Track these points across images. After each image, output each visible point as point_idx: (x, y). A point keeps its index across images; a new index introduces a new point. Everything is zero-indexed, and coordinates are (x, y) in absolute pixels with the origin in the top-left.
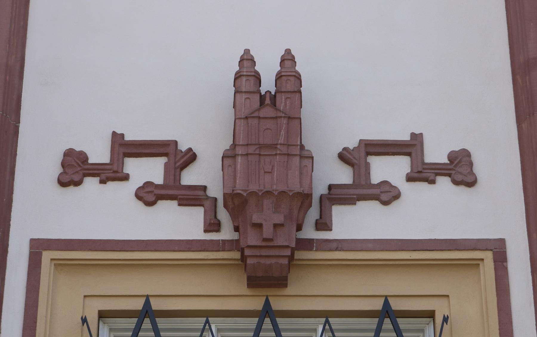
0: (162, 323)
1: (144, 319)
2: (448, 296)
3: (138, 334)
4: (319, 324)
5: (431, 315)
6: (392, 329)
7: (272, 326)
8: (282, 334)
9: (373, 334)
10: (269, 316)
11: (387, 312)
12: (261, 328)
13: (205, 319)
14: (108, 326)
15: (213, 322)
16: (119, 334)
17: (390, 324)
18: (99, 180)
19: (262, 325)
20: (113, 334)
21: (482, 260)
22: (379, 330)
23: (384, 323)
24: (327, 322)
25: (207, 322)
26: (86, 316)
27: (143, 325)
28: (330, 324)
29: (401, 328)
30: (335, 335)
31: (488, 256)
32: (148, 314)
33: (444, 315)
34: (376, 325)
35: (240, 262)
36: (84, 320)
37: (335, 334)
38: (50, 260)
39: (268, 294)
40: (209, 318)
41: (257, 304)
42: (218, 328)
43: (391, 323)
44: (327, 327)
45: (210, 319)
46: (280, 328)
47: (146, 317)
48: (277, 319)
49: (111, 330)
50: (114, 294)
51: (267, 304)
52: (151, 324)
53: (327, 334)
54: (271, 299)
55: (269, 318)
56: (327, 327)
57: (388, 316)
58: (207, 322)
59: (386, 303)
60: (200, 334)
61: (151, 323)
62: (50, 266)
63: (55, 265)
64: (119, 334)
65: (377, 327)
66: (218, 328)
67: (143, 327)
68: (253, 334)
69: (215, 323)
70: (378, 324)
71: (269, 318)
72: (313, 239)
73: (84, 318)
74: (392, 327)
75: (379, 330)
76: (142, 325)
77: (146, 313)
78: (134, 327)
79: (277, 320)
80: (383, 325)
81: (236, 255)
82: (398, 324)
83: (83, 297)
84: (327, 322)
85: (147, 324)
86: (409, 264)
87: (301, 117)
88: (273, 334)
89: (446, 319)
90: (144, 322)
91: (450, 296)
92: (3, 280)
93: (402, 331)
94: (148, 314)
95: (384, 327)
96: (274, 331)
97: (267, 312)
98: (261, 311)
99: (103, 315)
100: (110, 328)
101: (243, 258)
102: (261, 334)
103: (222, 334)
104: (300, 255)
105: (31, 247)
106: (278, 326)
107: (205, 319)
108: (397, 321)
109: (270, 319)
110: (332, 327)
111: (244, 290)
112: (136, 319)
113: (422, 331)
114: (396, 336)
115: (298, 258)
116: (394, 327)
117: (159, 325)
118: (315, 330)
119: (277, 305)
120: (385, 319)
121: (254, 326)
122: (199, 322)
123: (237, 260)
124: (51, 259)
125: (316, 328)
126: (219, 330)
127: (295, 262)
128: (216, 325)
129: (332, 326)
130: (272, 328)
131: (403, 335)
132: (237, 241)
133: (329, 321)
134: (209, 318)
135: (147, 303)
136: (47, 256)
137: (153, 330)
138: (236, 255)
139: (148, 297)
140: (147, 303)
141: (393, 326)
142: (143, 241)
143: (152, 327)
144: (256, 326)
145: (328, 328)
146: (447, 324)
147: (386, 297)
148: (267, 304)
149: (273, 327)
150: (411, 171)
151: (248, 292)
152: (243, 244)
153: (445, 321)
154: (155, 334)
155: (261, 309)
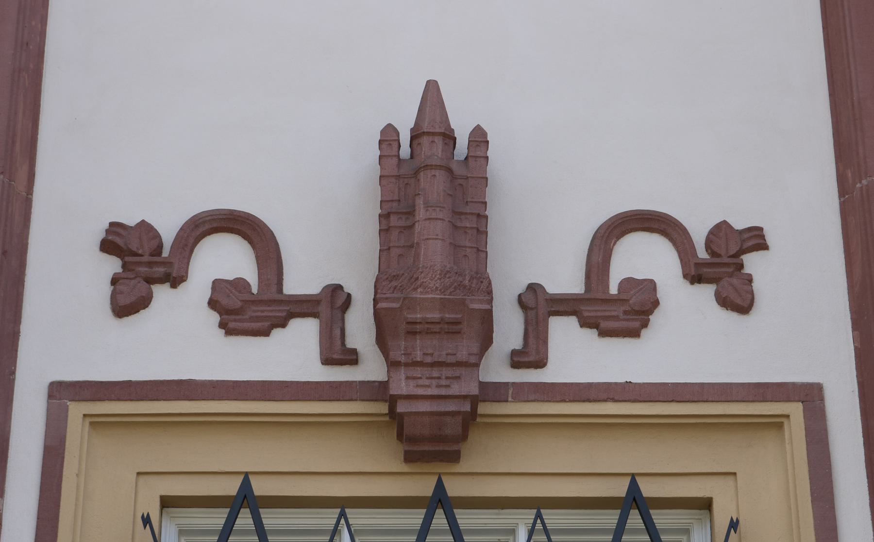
2: (735, 474)
3: (228, 539)
4: (522, 520)
5: (706, 505)
7: (448, 525)
8: (269, 538)
9: (610, 537)
10: (249, 506)
13: (338, 510)
14: (177, 526)
16: (590, 538)
18: (169, 285)
20: (185, 540)
21: (788, 416)
24: (539, 516)
25: (343, 515)
30: (551, 539)
31: (795, 410)
32: (441, 503)
35: (387, 419)
36: (147, 521)
37: (552, 537)
38: (82, 416)
39: (440, 471)
40: (542, 510)
41: (425, 488)
44: (539, 526)
47: (243, 507)
49: (182, 533)
51: (440, 486)
54: (444, 479)
55: (249, 508)
56: (539, 526)
58: (343, 515)
59: (634, 487)
60: (329, 538)
62: (83, 425)
63: (91, 423)
64: (590, 538)
65: (616, 526)
67: (236, 528)
68: (612, 537)
69: (358, 518)
70: (619, 519)
74: (643, 526)
77: (244, 499)
78: (221, 528)
79: (542, 513)
80: (537, 525)
82: (263, 524)
84: (539, 516)
85: (440, 520)
87: (488, 176)
88: (647, 538)
91: (738, 475)
93: (267, 532)
97: (440, 501)
98: (235, 496)
99: (167, 503)
100: (179, 530)
101: (392, 412)
102: (625, 538)
104: (484, 408)
107: (338, 510)
108: (345, 511)
112: (228, 510)
113: (687, 532)
114: (453, 540)
116: (645, 525)
118: (513, 532)
119: (455, 488)
122: (327, 518)
124: (85, 416)
125: (688, 529)
131: (463, 539)
132: (383, 385)
134: (542, 510)
135: (246, 485)
139: (246, 475)
140: (246, 485)
144: (617, 524)
145: (252, 528)
147: (633, 476)
148: (440, 486)
149: (449, 526)
151: (405, 468)
152: (394, 391)
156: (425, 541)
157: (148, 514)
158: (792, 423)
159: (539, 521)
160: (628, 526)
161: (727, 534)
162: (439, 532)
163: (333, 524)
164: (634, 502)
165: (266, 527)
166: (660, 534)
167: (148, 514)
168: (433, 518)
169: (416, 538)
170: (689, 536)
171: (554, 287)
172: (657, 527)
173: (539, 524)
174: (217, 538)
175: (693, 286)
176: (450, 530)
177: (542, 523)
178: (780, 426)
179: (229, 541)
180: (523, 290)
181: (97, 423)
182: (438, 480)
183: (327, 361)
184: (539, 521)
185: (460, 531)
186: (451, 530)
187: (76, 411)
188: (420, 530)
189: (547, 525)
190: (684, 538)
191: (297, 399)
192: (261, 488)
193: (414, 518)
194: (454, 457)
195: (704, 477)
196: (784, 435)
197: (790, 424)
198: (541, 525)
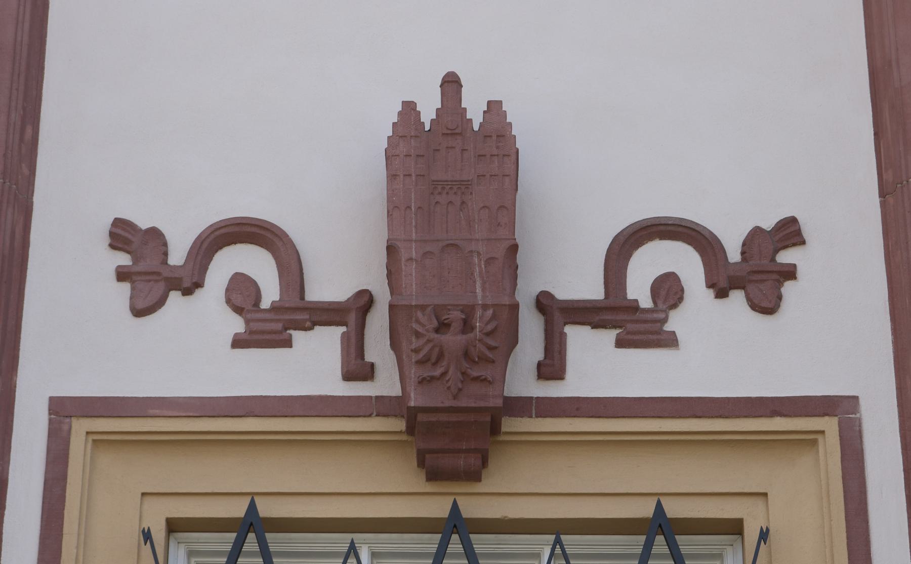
0: (481, 542)
1: (247, 535)
3: (237, 561)
4: (543, 544)
5: (735, 528)
6: (258, 551)
7: (668, 550)
11: (660, 526)
12: (445, 552)
13: (553, 537)
14: (186, 547)
15: (547, 543)
17: (459, 544)
19: (447, 547)
21: (823, 432)
22: (237, 551)
23: (654, 544)
24: (558, 541)
26: (151, 528)
27: (654, 549)
28: (563, 545)
29: (476, 552)
32: (253, 527)
33: (761, 527)
34: (232, 544)
35: (404, 437)
36: (147, 536)
38: (85, 434)
40: (561, 536)
41: (438, 508)
42: (372, 552)
43: (666, 543)
45: (563, 537)
46: (567, 552)
48: (677, 537)
49: (191, 554)
50: (563, 492)
51: (455, 507)
52: (259, 544)
53: (557, 562)
56: (558, 550)
57: (662, 533)
61: (258, 543)
62: (86, 440)
63: (94, 441)
64: (250, 560)
65: (232, 549)
66: (372, 552)
67: (245, 550)
70: (645, 546)
71: (663, 536)
72: (531, 398)
73: (146, 531)
75: (237, 551)
76: (243, 545)
78: (230, 550)
79: (562, 538)
80: (653, 547)
81: (399, 425)
83: (140, 495)
84: (558, 541)
85: (455, 545)
86: (704, 440)
89: (764, 535)
90: (246, 541)
92: (907, 471)
94: (253, 527)
95: (655, 550)
96: (355, 557)
97: (455, 526)
98: (447, 518)
99: (174, 526)
100: (189, 550)
103: (196, 560)
104: (510, 424)
105: (51, 411)
106: (268, 546)
107: (553, 537)
109: (665, 537)
110: (565, 551)
111: (419, 483)
113: (720, 557)
115: (508, 430)
116: (670, 551)
117: (476, 548)
118: (538, 556)
119: (472, 509)
120: (657, 536)
121: (228, 548)
123: (401, 432)
124: (88, 433)
126: (374, 555)
127: (502, 438)
128: (369, 547)
129: (681, 550)
130: (464, 551)
133: (561, 541)
134: (561, 536)
136: (80, 428)
137: (564, 555)
138: (399, 425)
139: (253, 495)
140: (252, 507)
141: (669, 548)
142: (692, 397)
143: (259, 550)
145: (257, 550)
146: (765, 544)
148: (455, 507)
149: (464, 550)
150: (280, 299)
153: (762, 538)
154: (264, 561)
155: (447, 516)
156: (236, 562)
157: (149, 528)
158: (827, 440)
159: (558, 546)
160: (246, 546)
161: (157, 559)
162: (251, 554)
163: (435, 548)
164: (659, 528)
165: (666, 549)
166: (272, 555)
167: (149, 528)
168: (244, 542)
169: (342, 561)
170: (722, 561)
171: (564, 293)
172: (271, 550)
173: (558, 548)
174: (226, 560)
175: (183, 297)
176: (670, 555)
177: (564, 549)
178: (814, 442)
179: (238, 563)
180: (733, 293)
181: (100, 442)
182: (251, 500)
183: (348, 376)
184: (558, 546)
185: (683, 557)
186: (466, 554)
187: (80, 428)
188: (642, 554)
189: (475, 549)
190: (718, 563)
191: (591, 415)
192: (267, 509)
193: (430, 542)
194: (474, 476)
195: (371, 498)
196: (818, 452)
197: (825, 441)
198: (560, 550)
